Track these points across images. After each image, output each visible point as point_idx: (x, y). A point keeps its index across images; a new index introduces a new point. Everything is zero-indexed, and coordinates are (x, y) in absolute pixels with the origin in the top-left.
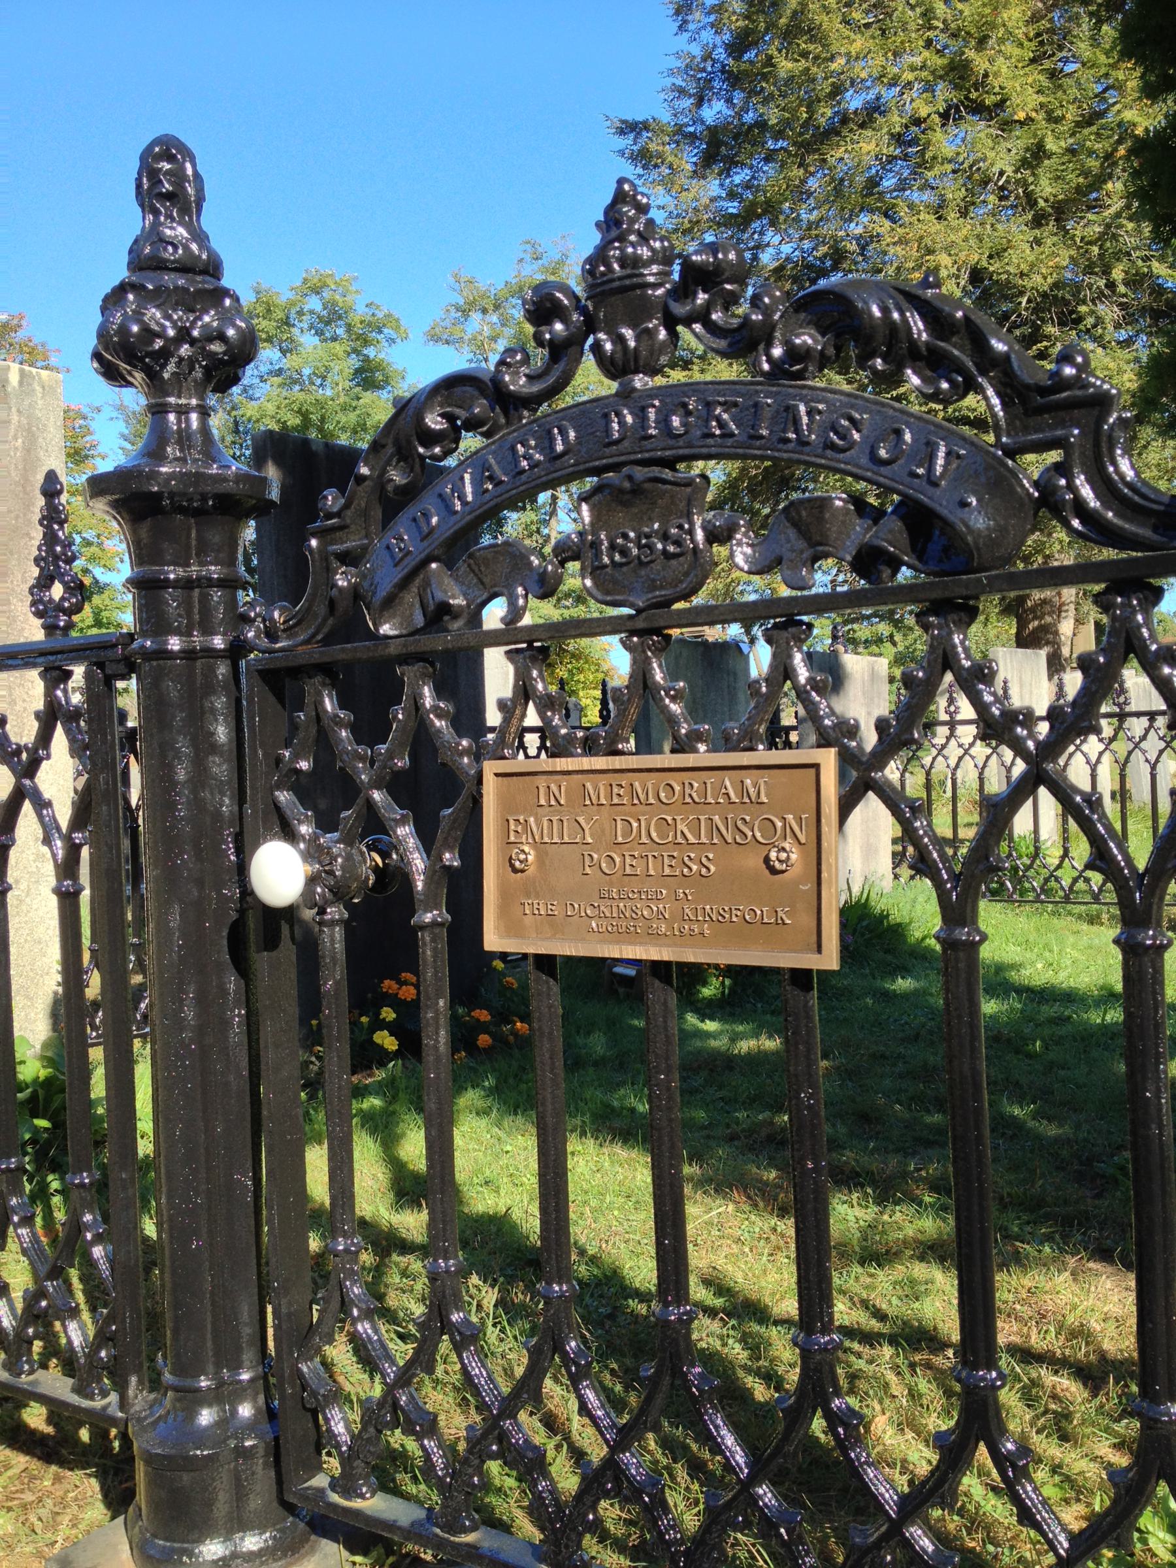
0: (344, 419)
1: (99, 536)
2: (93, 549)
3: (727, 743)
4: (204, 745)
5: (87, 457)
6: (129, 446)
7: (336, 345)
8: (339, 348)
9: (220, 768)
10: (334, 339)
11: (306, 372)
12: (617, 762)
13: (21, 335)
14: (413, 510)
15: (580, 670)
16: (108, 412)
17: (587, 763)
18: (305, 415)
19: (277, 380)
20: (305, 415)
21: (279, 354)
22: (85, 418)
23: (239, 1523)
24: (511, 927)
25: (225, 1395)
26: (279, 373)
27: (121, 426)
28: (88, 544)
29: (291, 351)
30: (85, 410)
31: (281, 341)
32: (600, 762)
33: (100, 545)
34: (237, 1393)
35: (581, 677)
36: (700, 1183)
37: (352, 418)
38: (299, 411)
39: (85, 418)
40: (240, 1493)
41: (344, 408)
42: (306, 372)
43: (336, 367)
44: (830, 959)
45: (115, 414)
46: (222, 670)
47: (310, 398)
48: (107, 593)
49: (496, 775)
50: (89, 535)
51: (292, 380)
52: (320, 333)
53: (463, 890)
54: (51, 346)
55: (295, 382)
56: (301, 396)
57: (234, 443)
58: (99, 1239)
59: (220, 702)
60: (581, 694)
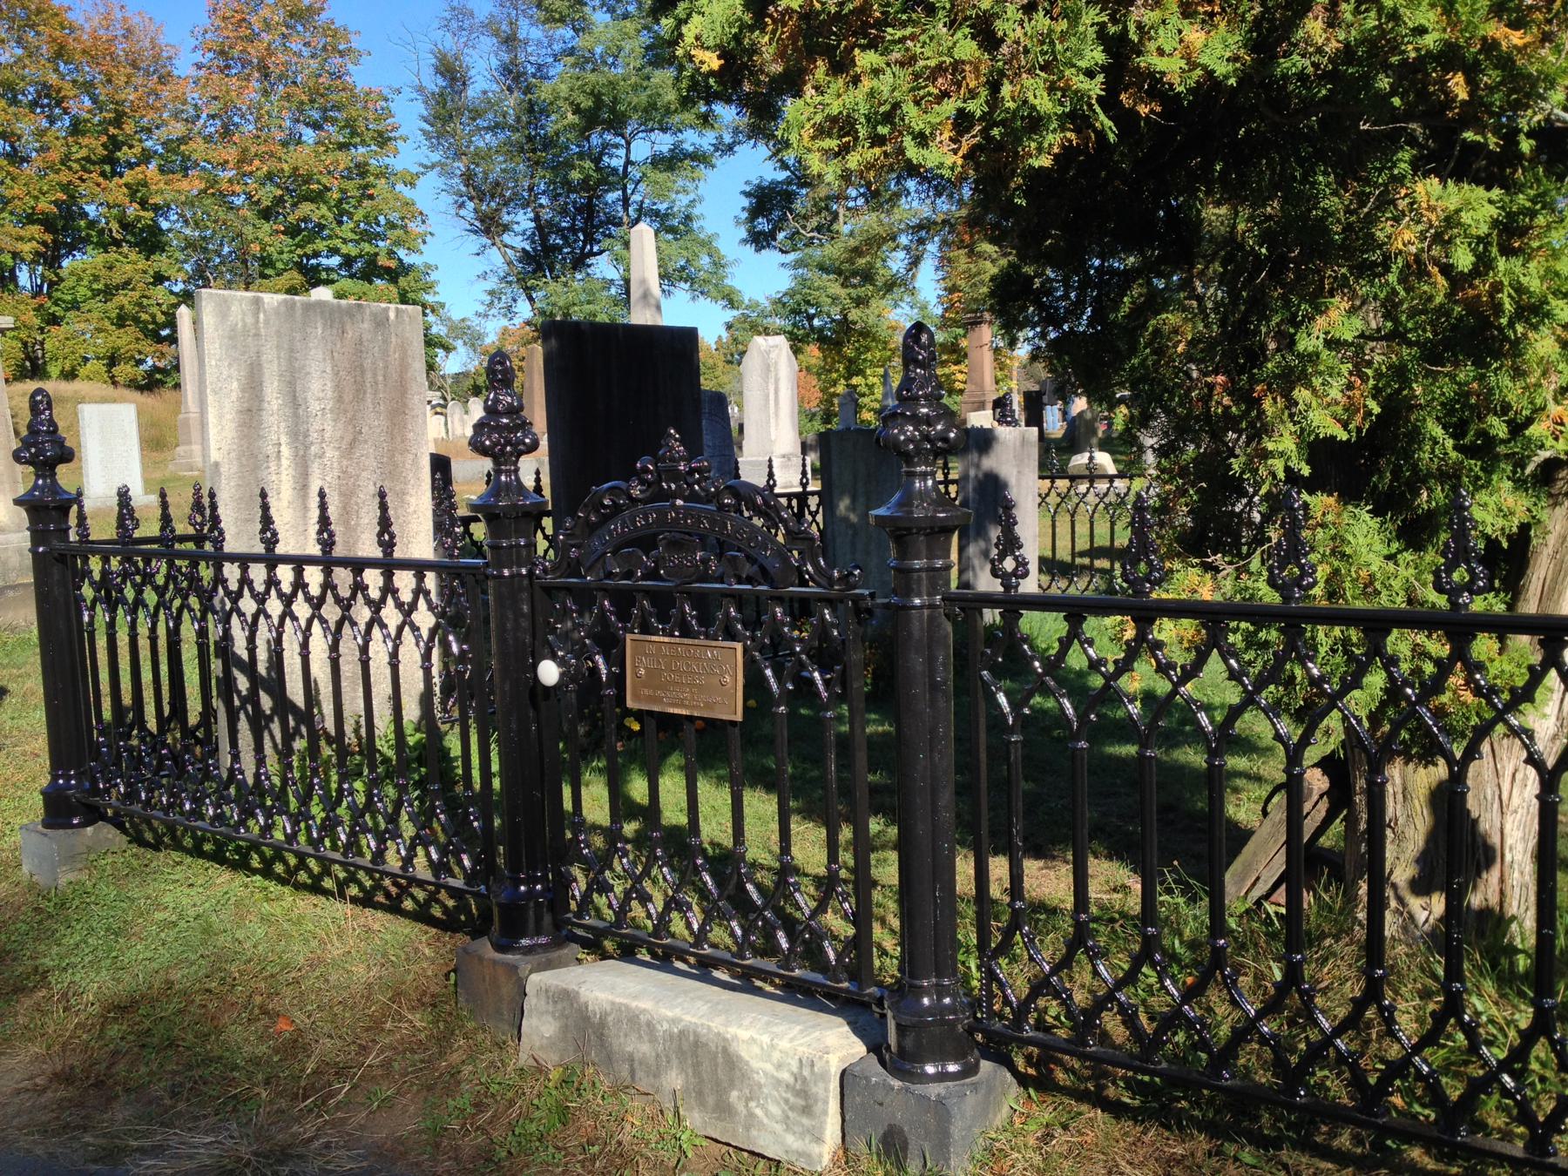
0: (635, 100)
1: (402, 219)
2: (399, 232)
3: (707, 637)
4: (518, 614)
5: (390, 139)
6: (428, 128)
7: (628, 23)
8: (629, 26)
9: (525, 624)
10: (626, 16)
11: (598, 50)
12: (673, 640)
13: (324, 16)
14: (599, 532)
15: (868, 349)
16: (408, 93)
17: (662, 639)
18: (597, 97)
19: (570, 60)
20: (597, 97)
21: (572, 33)
22: (386, 100)
23: (538, 933)
24: (636, 697)
25: (531, 881)
26: (571, 52)
27: (421, 108)
28: (392, 226)
29: (583, 29)
30: (385, 92)
31: (573, 20)
32: (666, 639)
33: (404, 227)
34: (536, 881)
35: (869, 356)
36: (799, 811)
37: (643, 98)
38: (592, 93)
39: (386, 100)
40: (539, 919)
41: (635, 88)
42: (598, 50)
43: (627, 46)
44: (739, 717)
45: (415, 95)
46: (526, 582)
47: (602, 80)
48: (412, 275)
49: (770, 461)
50: (394, 217)
51: (585, 61)
52: (611, 10)
53: (619, 681)
54: (351, 28)
55: (587, 61)
56: (592, 77)
57: (529, 123)
58: (476, 819)
59: (525, 595)
60: (868, 372)
